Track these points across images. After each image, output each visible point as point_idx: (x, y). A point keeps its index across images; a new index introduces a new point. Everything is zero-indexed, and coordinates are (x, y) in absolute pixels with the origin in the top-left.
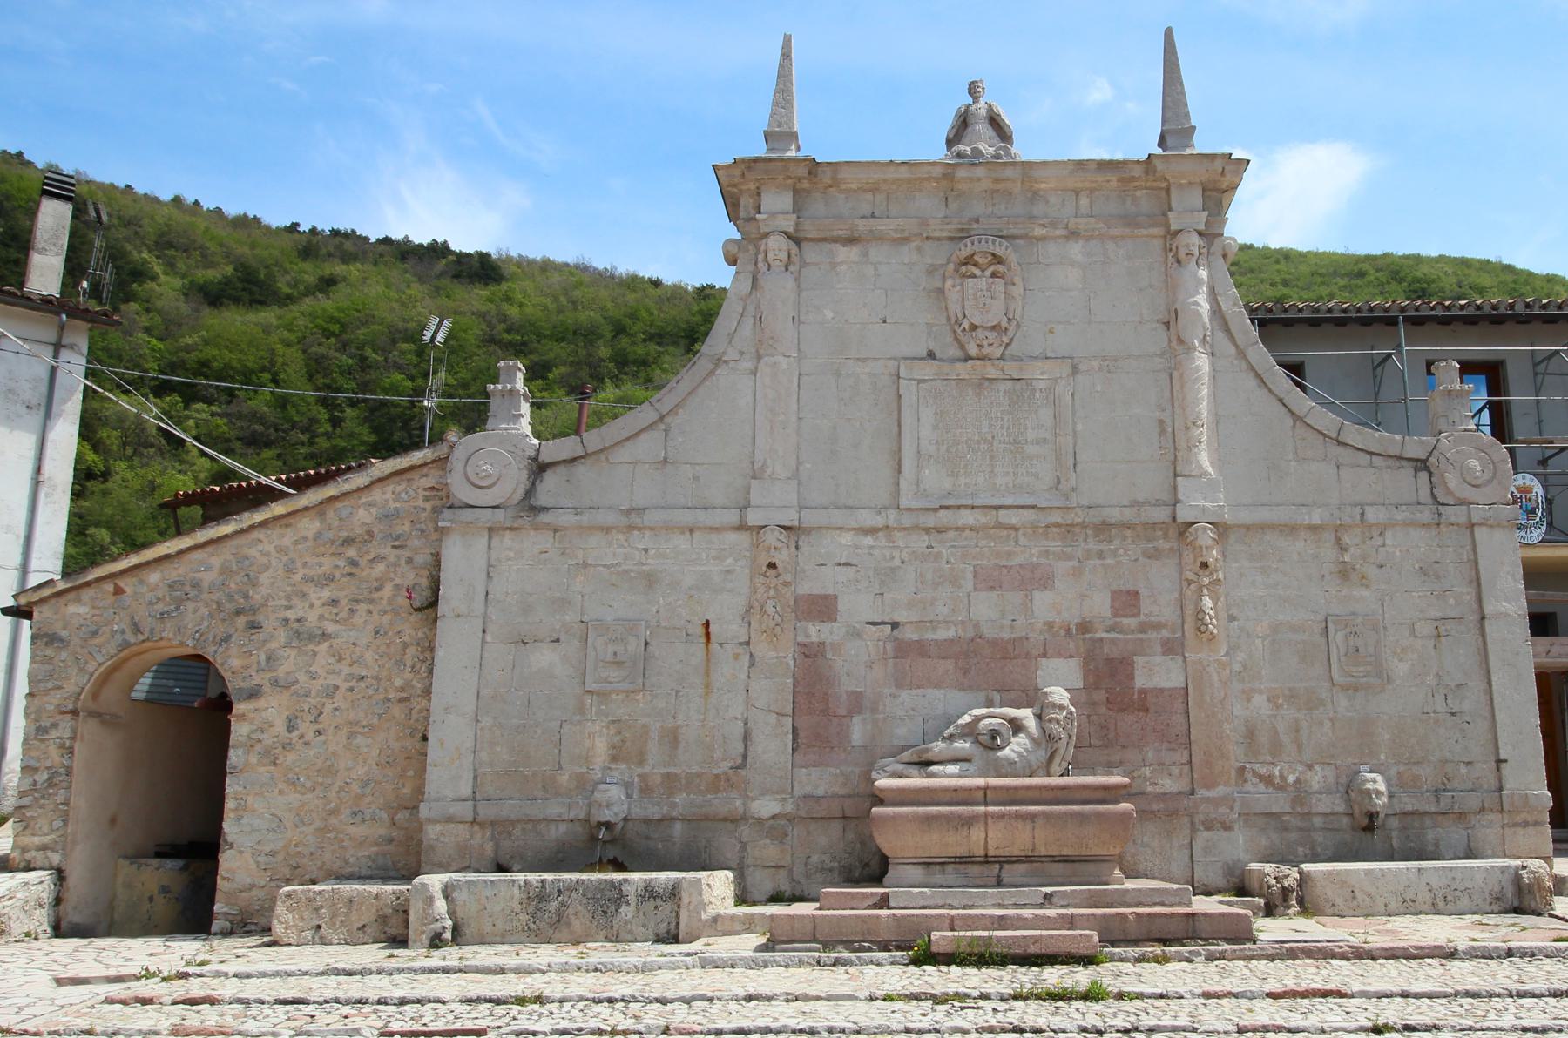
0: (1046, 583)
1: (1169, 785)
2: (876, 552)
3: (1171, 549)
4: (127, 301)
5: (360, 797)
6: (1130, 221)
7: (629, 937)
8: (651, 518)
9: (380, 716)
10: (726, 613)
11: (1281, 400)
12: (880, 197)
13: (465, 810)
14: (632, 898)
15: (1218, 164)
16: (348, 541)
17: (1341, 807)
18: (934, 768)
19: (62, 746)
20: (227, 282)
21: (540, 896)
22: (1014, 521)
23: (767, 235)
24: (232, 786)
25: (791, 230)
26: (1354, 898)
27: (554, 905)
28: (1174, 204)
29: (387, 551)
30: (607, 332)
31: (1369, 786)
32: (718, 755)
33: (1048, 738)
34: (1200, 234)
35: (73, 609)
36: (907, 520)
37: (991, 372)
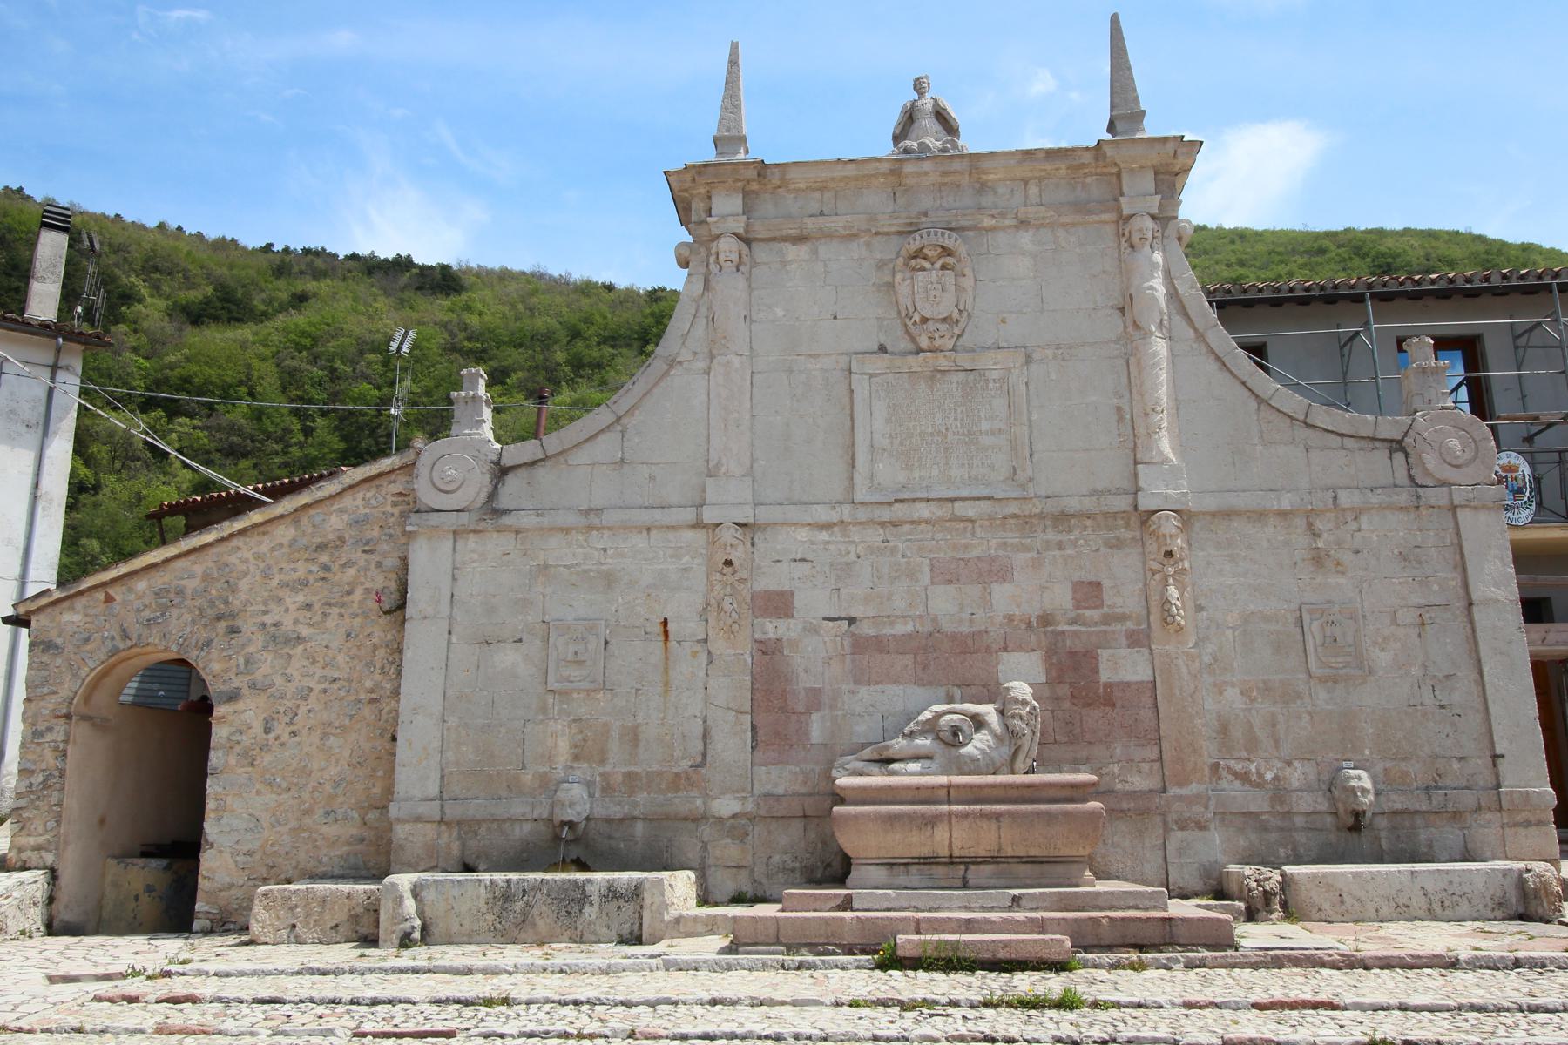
0: (1004, 575)
1: (1139, 782)
2: (832, 547)
3: (1133, 538)
4: (117, 323)
5: (332, 797)
6: (1080, 208)
7: (593, 938)
8: (609, 518)
10: (683, 610)
11: (1244, 383)
12: (828, 195)
13: (432, 810)
14: (596, 898)
15: (1170, 147)
16: (321, 547)
17: (1324, 806)
18: (895, 766)
19: (56, 749)
20: (207, 302)
21: (505, 896)
23: (718, 237)
24: (212, 787)
25: (741, 231)
26: (1342, 902)
27: (519, 905)
28: (1125, 189)
29: (357, 556)
30: (563, 337)
31: (1353, 783)
33: (1011, 734)
34: (1153, 217)
35: (67, 617)
36: (862, 515)
37: (943, 363)
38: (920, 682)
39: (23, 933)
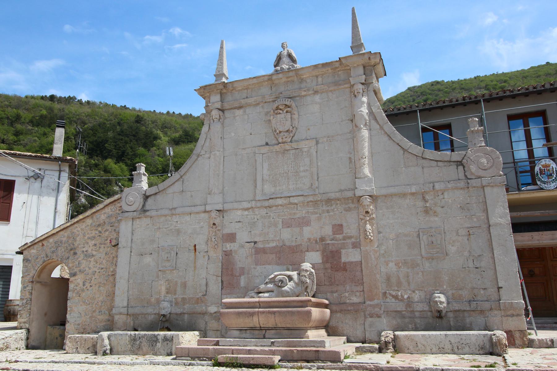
0: (308, 223)
1: (355, 300)
3: (355, 207)
4: (153, 147)
5: (101, 307)
6: (336, 83)
8: (178, 211)
9: (107, 280)
10: (200, 241)
11: (398, 144)
13: (124, 311)
16: (99, 225)
17: (426, 308)
18: (261, 295)
20: (181, 137)
21: (134, 339)
22: (296, 201)
24: (69, 304)
25: (219, 107)
26: (417, 346)
27: (138, 342)
28: (352, 75)
29: (109, 228)
31: (437, 299)
32: (198, 291)
33: (301, 283)
34: (363, 84)
36: (259, 204)
37: (287, 147)
38: (278, 264)
39: (17, 348)
